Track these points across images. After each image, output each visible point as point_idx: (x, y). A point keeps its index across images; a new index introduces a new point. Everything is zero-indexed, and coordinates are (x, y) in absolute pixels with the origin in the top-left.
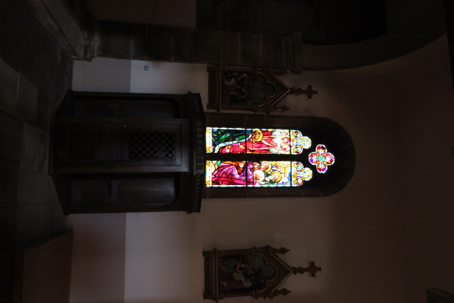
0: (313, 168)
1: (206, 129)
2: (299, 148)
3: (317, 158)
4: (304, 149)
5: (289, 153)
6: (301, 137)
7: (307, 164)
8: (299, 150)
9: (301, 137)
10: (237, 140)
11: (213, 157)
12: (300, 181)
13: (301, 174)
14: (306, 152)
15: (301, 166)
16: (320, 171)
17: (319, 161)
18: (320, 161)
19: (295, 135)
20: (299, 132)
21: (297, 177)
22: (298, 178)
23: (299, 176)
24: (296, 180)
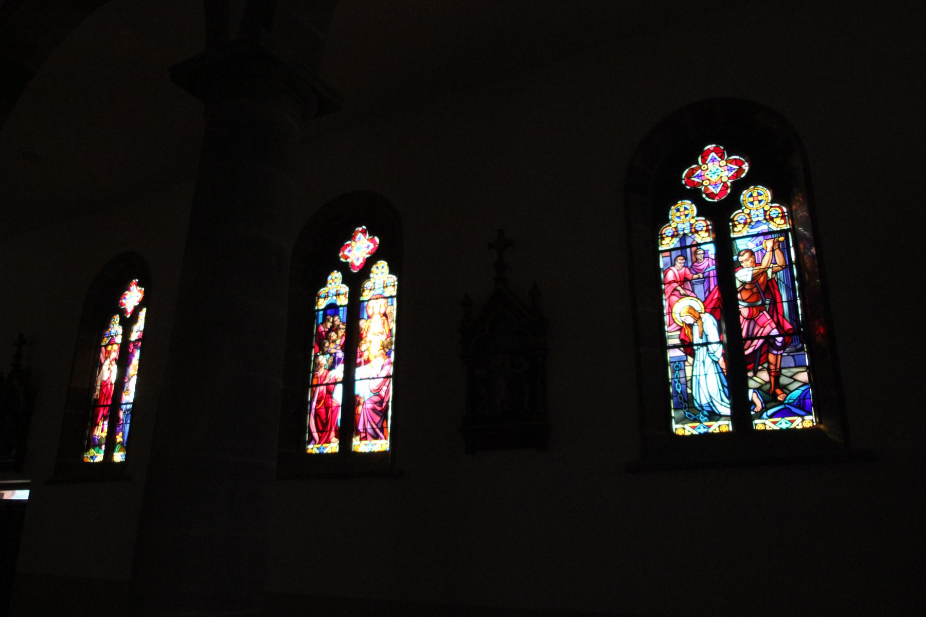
0: (739, 185)
1: (308, 449)
2: (771, 213)
3: (716, 185)
4: (698, 215)
5: (395, 300)
6: (743, 212)
7: (732, 202)
8: (777, 212)
9: (743, 212)
10: (752, 363)
11: (345, 444)
12: (775, 211)
13: (757, 214)
14: (704, 210)
15: (738, 216)
16: (744, 170)
17: (721, 177)
18: (720, 176)
19: (742, 226)
20: (662, 231)
21: (765, 219)
22: (768, 217)
23: (763, 217)
24: (773, 221)
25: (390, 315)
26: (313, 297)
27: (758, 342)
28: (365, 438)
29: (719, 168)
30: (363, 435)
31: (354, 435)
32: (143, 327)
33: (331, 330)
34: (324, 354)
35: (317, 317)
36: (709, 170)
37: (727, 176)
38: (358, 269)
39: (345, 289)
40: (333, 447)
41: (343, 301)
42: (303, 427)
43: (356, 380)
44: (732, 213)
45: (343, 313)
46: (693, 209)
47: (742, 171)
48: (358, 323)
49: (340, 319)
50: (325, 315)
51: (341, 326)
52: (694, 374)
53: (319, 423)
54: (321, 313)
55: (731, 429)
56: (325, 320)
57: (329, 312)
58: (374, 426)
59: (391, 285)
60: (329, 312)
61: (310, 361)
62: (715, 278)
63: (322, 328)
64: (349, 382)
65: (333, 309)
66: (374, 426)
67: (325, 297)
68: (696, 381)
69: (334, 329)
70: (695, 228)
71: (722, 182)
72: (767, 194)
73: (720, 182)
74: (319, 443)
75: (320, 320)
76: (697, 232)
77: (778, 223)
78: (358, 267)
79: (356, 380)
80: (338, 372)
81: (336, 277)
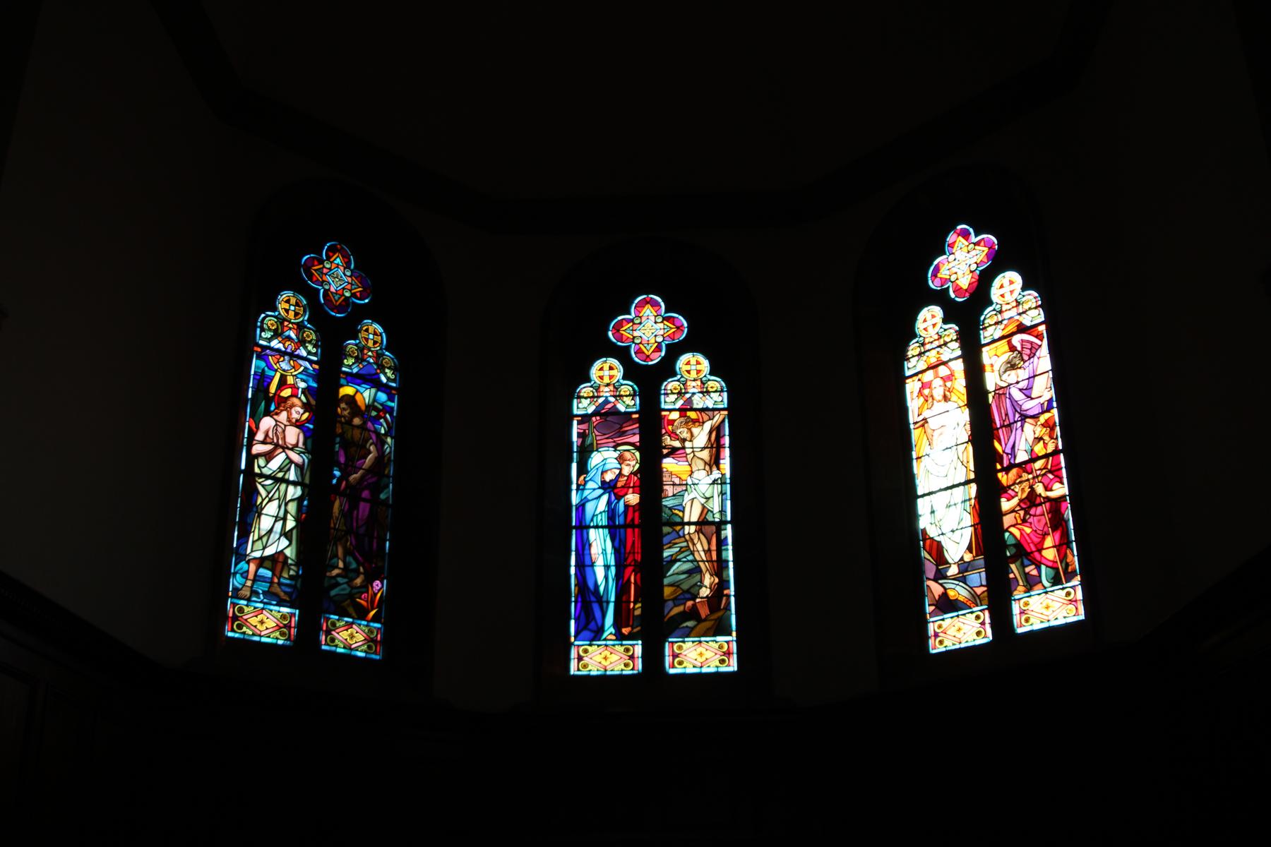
0: (675, 351)
14: (631, 371)
25: (674, 391)
27: (1031, 571)
29: (654, 324)
32: (688, 354)
36: (642, 325)
37: (976, 263)
38: (967, 294)
44: (578, 387)
46: (619, 373)
47: (679, 328)
55: (1020, 631)
59: (952, 341)
70: (707, 388)
71: (656, 342)
72: (705, 365)
73: (653, 341)
76: (708, 392)
77: (627, 403)
78: (966, 290)
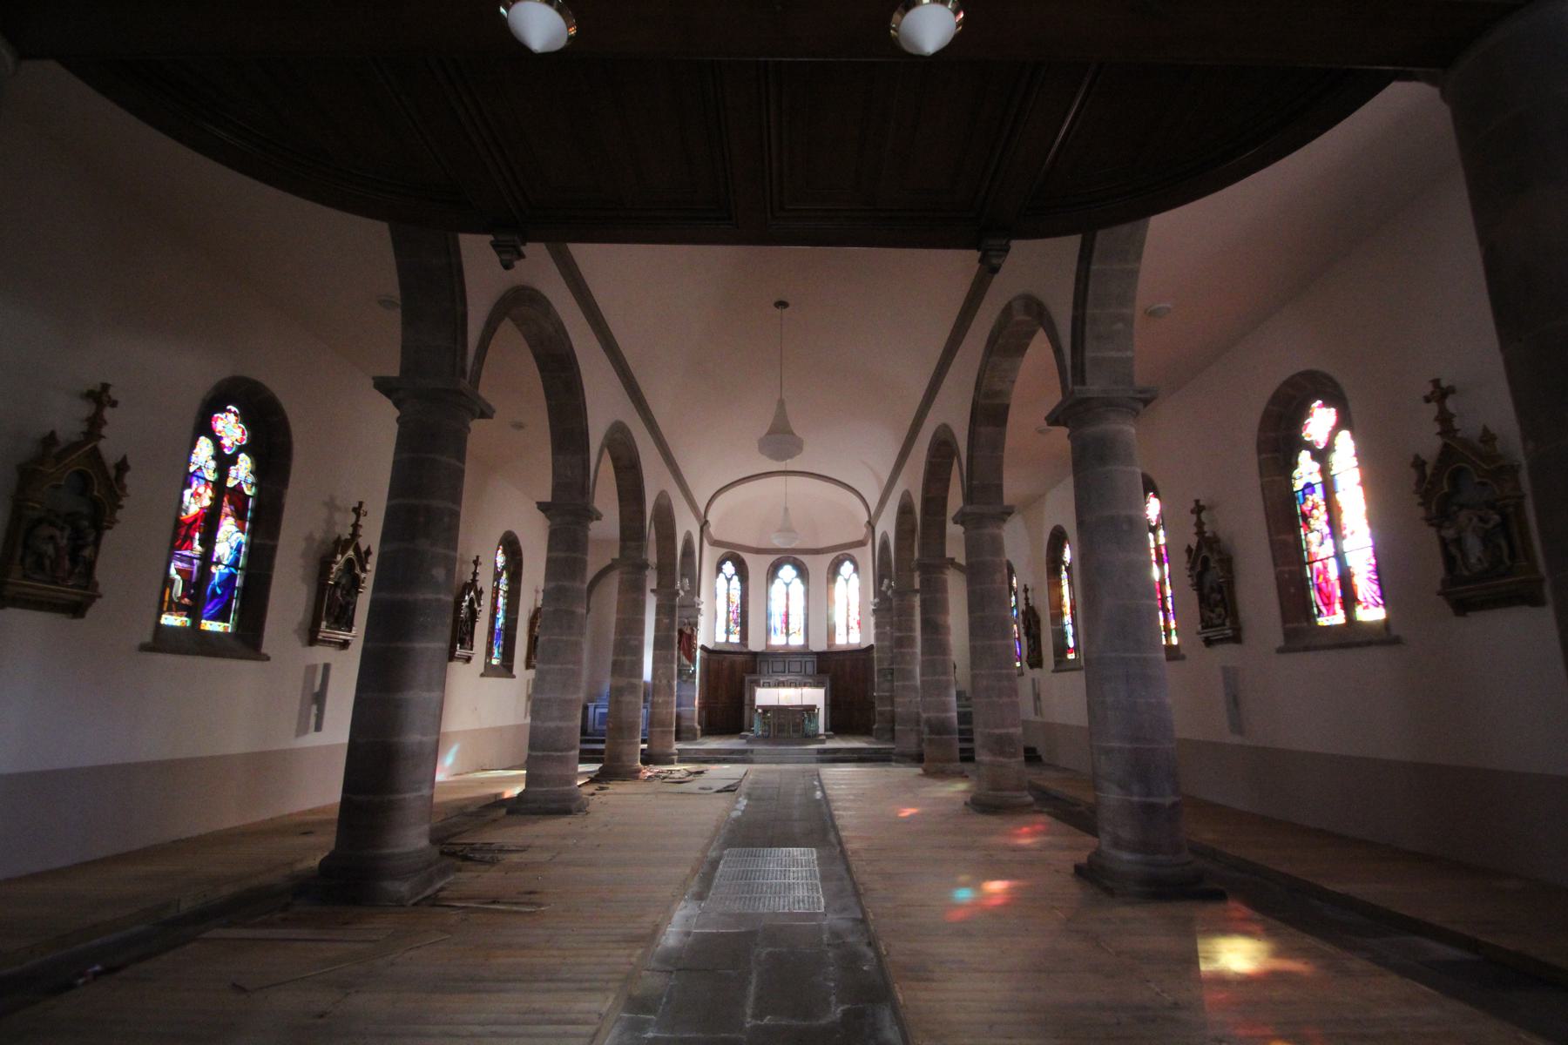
26: (1289, 479)
28: (1366, 608)
30: (1364, 604)
31: (900, 9)
33: (1313, 508)
34: (1312, 532)
35: (1298, 498)
39: (1316, 466)
40: (1339, 618)
41: (1316, 479)
42: (1308, 603)
43: (848, 642)
45: (1319, 488)
48: (1347, 429)
49: (1318, 496)
50: (1304, 495)
51: (1320, 503)
52: (731, 610)
53: (1324, 598)
54: (1300, 493)
56: (1305, 500)
57: (1306, 491)
58: (1374, 595)
60: (1306, 491)
61: (1301, 540)
62: (1306, 560)
63: (1305, 508)
64: (1339, 556)
65: (1309, 487)
66: (1374, 595)
67: (1301, 477)
68: (327, 633)
69: (1314, 507)
74: (1328, 615)
75: (1301, 501)
79: (848, 642)
80: (1328, 549)
81: (1304, 457)
